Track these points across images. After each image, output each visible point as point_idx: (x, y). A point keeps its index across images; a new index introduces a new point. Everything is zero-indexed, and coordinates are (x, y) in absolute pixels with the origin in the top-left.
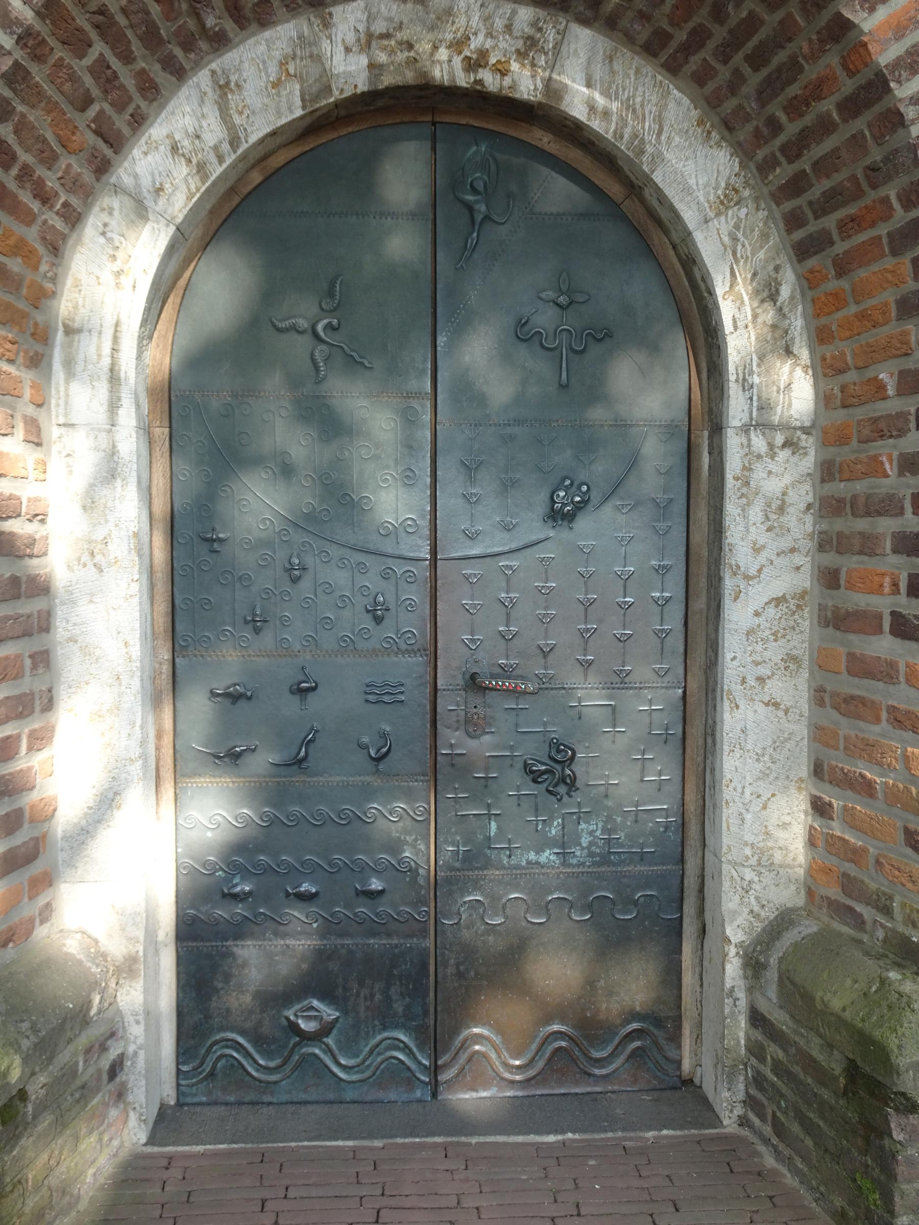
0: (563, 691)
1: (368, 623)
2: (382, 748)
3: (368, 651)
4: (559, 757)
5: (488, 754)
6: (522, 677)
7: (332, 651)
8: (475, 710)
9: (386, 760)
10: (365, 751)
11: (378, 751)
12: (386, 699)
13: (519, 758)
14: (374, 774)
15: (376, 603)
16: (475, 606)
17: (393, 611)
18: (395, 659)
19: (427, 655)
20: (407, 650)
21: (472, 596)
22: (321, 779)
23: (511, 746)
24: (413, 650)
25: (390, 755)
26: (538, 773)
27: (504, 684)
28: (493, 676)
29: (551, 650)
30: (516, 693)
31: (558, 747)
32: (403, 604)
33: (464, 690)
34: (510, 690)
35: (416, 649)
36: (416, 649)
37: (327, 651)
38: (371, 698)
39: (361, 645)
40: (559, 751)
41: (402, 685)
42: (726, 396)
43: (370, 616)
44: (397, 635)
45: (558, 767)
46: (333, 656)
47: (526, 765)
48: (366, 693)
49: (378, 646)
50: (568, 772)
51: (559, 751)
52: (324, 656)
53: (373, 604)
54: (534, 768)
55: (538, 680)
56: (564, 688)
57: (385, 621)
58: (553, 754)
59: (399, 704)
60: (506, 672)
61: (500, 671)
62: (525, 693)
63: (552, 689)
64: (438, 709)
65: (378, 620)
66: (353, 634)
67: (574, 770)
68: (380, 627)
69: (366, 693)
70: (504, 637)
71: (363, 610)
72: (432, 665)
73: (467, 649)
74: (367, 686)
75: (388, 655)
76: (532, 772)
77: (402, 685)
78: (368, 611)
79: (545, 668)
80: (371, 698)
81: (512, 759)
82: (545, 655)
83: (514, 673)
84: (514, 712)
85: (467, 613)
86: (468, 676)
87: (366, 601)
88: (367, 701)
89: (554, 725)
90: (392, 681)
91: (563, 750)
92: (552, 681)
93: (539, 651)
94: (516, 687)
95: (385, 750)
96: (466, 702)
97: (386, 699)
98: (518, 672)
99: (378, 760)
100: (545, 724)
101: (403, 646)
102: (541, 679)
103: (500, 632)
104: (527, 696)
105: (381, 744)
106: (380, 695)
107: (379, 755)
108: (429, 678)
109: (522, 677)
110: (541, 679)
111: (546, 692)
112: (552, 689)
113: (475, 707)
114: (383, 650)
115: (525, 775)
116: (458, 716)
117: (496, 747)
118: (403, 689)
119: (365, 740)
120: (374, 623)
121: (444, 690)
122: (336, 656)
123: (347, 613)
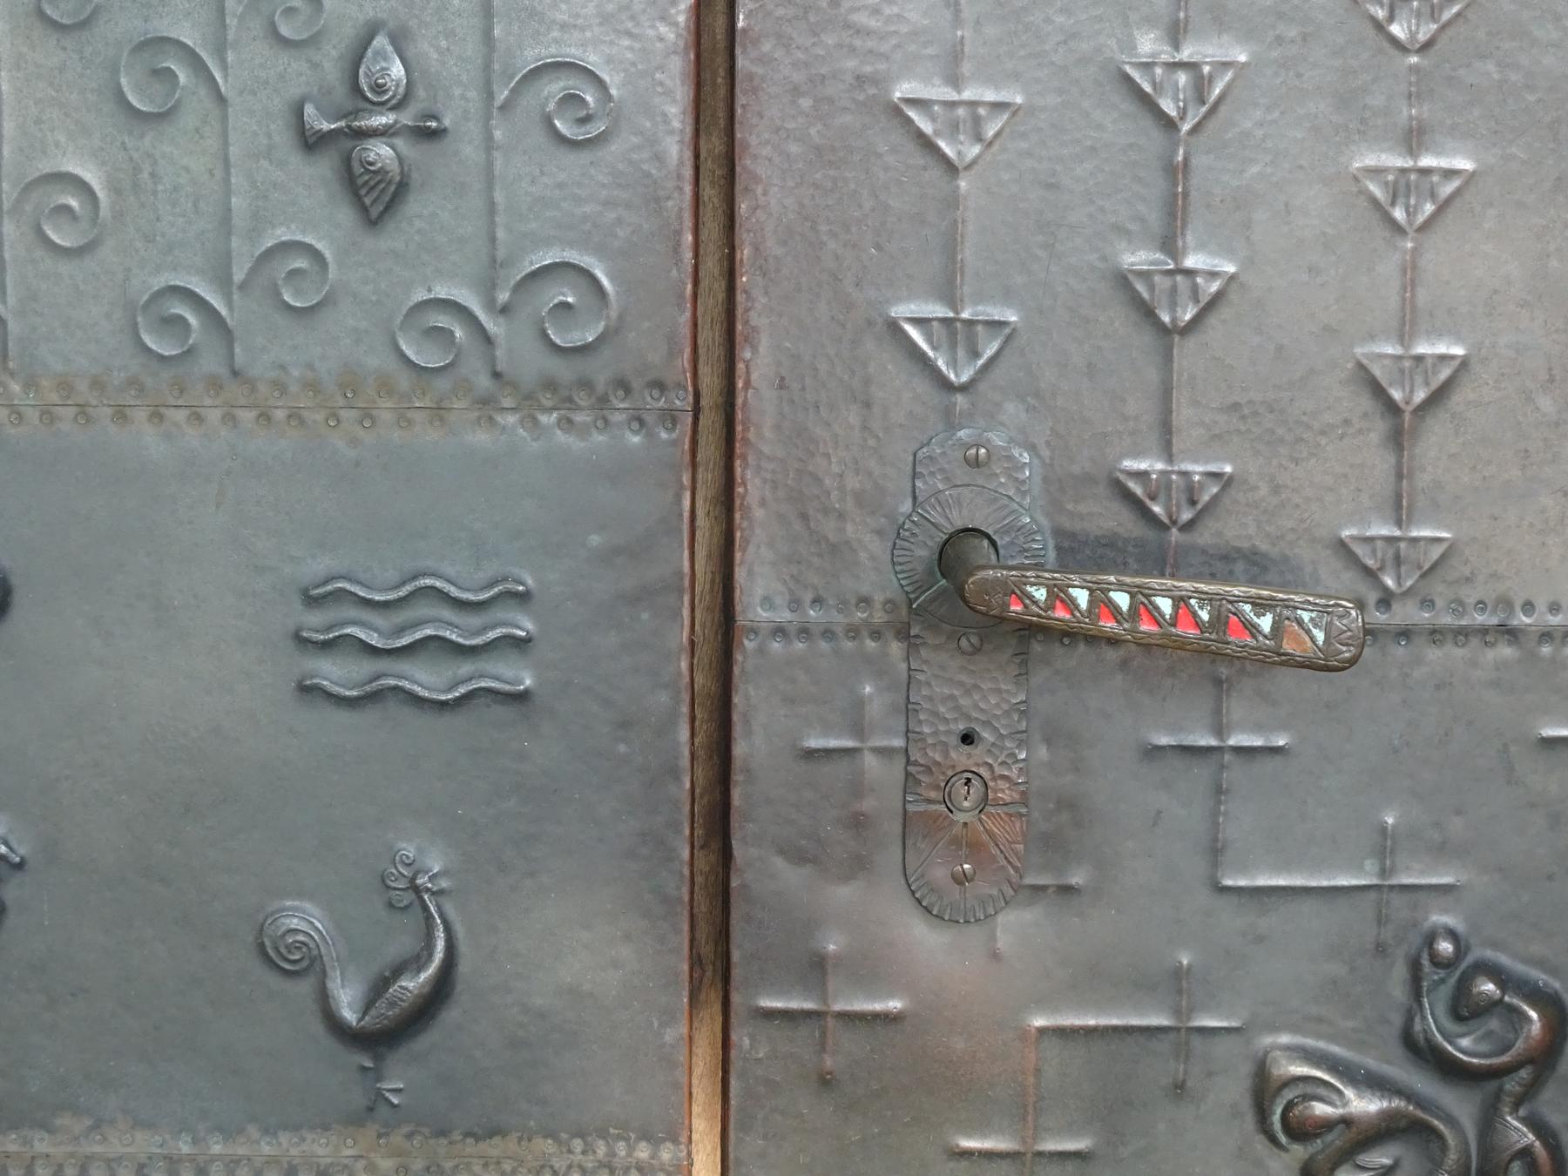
0: (1506, 651)
1: (311, 212)
2: (398, 971)
3: (313, 386)
4: (1465, 1046)
5: (1039, 1022)
6: (1256, 565)
7: (97, 384)
8: (962, 757)
9: (423, 1042)
10: (304, 988)
11: (379, 987)
12: (424, 678)
13: (1221, 1047)
14: (357, 1119)
15: (359, 94)
16: (972, 119)
17: (469, 150)
18: (481, 438)
19: (670, 417)
20: (551, 385)
21: (955, 56)
22: (42, 1144)
23: (1178, 974)
24: (586, 384)
25: (450, 1015)
26: (1335, 1139)
27: (1142, 605)
28: (1081, 553)
29: (1438, 397)
30: (1216, 663)
31: (1464, 985)
32: (528, 101)
33: (903, 634)
34: (1181, 644)
35: (601, 381)
36: (601, 381)
37: (65, 386)
38: (335, 672)
39: (269, 349)
40: (1465, 1010)
41: (524, 598)
42: (433, 1017)
43: (324, 167)
44: (488, 289)
45: (1460, 1105)
46: (386, 410)
47: (1263, 1088)
48: (301, 641)
49: (376, 360)
50: (1519, 1133)
51: (1465, 1010)
52: (48, 415)
53: (341, 93)
54: (1320, 1109)
55: (1349, 579)
56: (1511, 633)
57: (415, 206)
58: (1434, 1022)
59: (501, 711)
60: (1152, 536)
61: (1113, 519)
62: (1274, 659)
63: (1436, 635)
64: (739, 749)
65: (375, 199)
66: (223, 282)
67: (1555, 1119)
68: (390, 240)
69: (301, 641)
70: (1147, 312)
71: (282, 136)
72: (709, 478)
73: (922, 386)
74: (312, 601)
75: (439, 411)
76: (1300, 1131)
77: (524, 598)
78: (311, 143)
79: (1400, 510)
80: (335, 672)
81: (1183, 1052)
82: (1399, 427)
83: (1204, 536)
84: (1201, 772)
85: (919, 159)
86: (923, 552)
87: (297, 76)
88: (308, 690)
89: (1442, 850)
90: (460, 574)
91: (1493, 1006)
92: (1439, 591)
93: (1366, 402)
94: (1219, 622)
95: (414, 984)
96: (908, 709)
97: (424, 678)
98: (1234, 528)
99: (377, 1041)
100: (1385, 847)
101: (528, 362)
102: (1370, 574)
103: (1123, 280)
104: (1287, 680)
105: (402, 944)
106: (371, 654)
107: (384, 1013)
108: (683, 559)
109: (1256, 565)
110: (1370, 574)
111: (1400, 651)
112: (1436, 635)
113: (967, 738)
114: (404, 381)
115: (1260, 1144)
116: (857, 788)
117: (1091, 980)
118: (524, 624)
119: (304, 919)
120: (346, 215)
121: (779, 631)
122: (121, 415)
123: (182, 155)
